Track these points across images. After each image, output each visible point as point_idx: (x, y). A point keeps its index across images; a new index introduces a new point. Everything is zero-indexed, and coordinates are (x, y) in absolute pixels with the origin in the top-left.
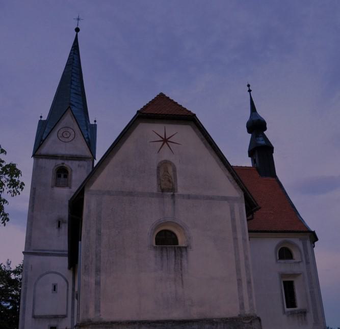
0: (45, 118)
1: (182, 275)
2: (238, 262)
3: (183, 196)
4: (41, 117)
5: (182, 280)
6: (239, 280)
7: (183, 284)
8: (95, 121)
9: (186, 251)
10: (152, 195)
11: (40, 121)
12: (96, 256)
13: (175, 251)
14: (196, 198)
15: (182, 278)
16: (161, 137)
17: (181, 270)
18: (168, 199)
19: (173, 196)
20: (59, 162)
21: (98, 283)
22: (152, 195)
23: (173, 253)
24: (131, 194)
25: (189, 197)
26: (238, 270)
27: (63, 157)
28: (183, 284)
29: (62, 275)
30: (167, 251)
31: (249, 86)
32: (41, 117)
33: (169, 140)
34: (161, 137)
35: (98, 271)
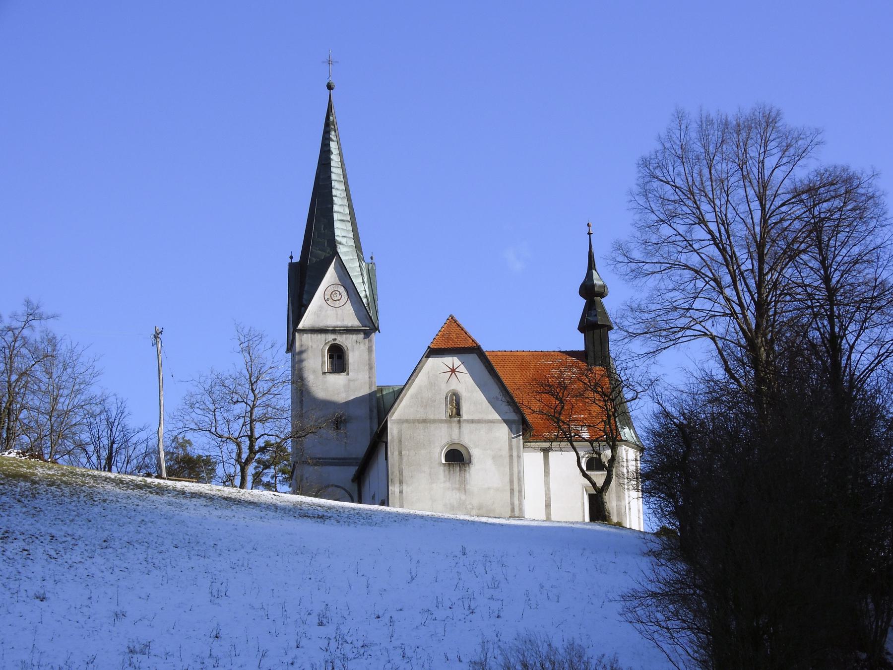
0: (297, 259)
1: (465, 486)
2: (511, 475)
3: (468, 421)
4: (291, 257)
5: (465, 490)
6: (512, 490)
7: (465, 492)
8: (372, 258)
9: (469, 466)
10: (441, 421)
11: (291, 265)
12: (399, 472)
13: (460, 467)
14: (479, 421)
15: (465, 488)
16: (449, 368)
17: (464, 481)
18: (455, 426)
19: (459, 421)
20: (330, 337)
21: (401, 492)
22: (441, 421)
23: (459, 468)
24: (424, 421)
25: (472, 421)
26: (511, 482)
27: (334, 331)
28: (465, 492)
29: (344, 489)
30: (453, 466)
31: (588, 225)
32: (291, 257)
33: (456, 370)
34: (449, 368)
35: (401, 482)
